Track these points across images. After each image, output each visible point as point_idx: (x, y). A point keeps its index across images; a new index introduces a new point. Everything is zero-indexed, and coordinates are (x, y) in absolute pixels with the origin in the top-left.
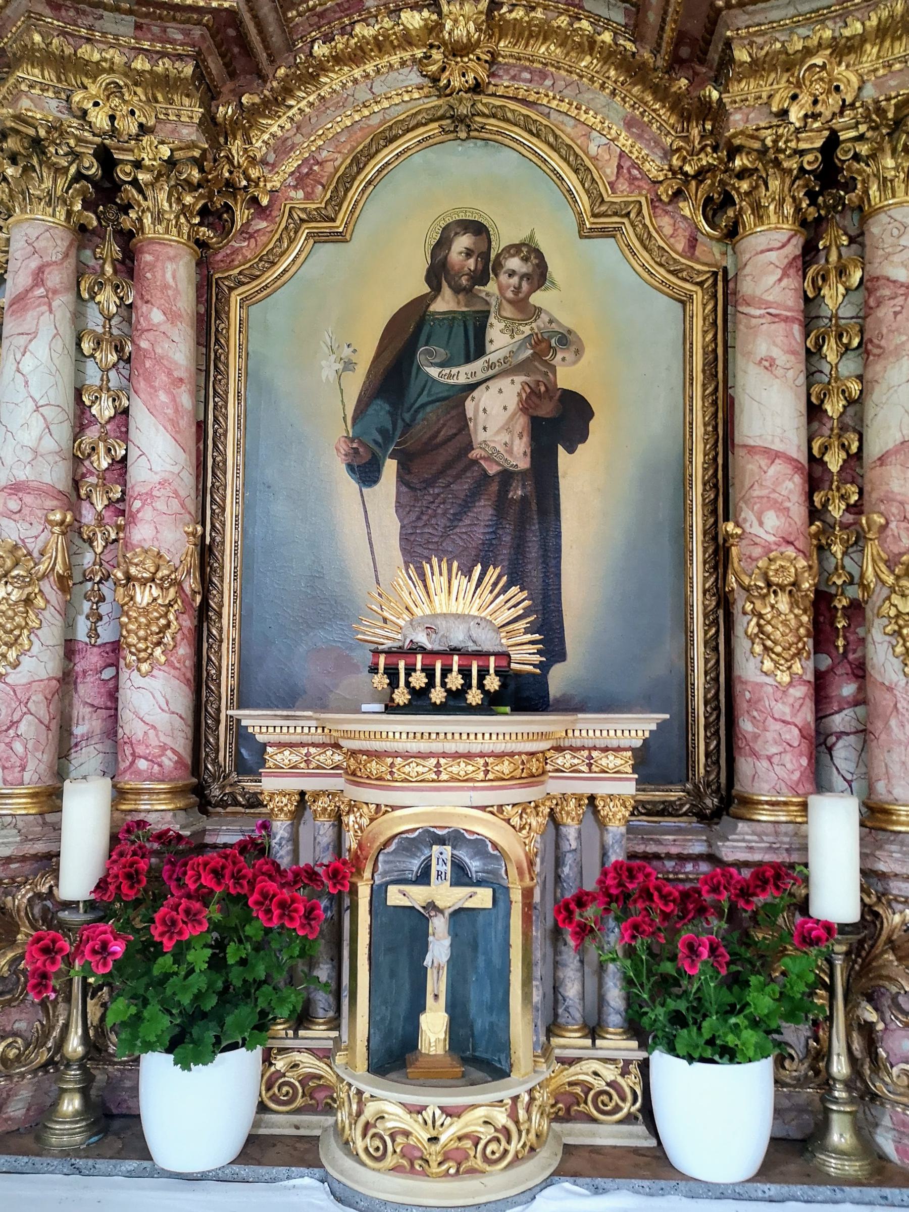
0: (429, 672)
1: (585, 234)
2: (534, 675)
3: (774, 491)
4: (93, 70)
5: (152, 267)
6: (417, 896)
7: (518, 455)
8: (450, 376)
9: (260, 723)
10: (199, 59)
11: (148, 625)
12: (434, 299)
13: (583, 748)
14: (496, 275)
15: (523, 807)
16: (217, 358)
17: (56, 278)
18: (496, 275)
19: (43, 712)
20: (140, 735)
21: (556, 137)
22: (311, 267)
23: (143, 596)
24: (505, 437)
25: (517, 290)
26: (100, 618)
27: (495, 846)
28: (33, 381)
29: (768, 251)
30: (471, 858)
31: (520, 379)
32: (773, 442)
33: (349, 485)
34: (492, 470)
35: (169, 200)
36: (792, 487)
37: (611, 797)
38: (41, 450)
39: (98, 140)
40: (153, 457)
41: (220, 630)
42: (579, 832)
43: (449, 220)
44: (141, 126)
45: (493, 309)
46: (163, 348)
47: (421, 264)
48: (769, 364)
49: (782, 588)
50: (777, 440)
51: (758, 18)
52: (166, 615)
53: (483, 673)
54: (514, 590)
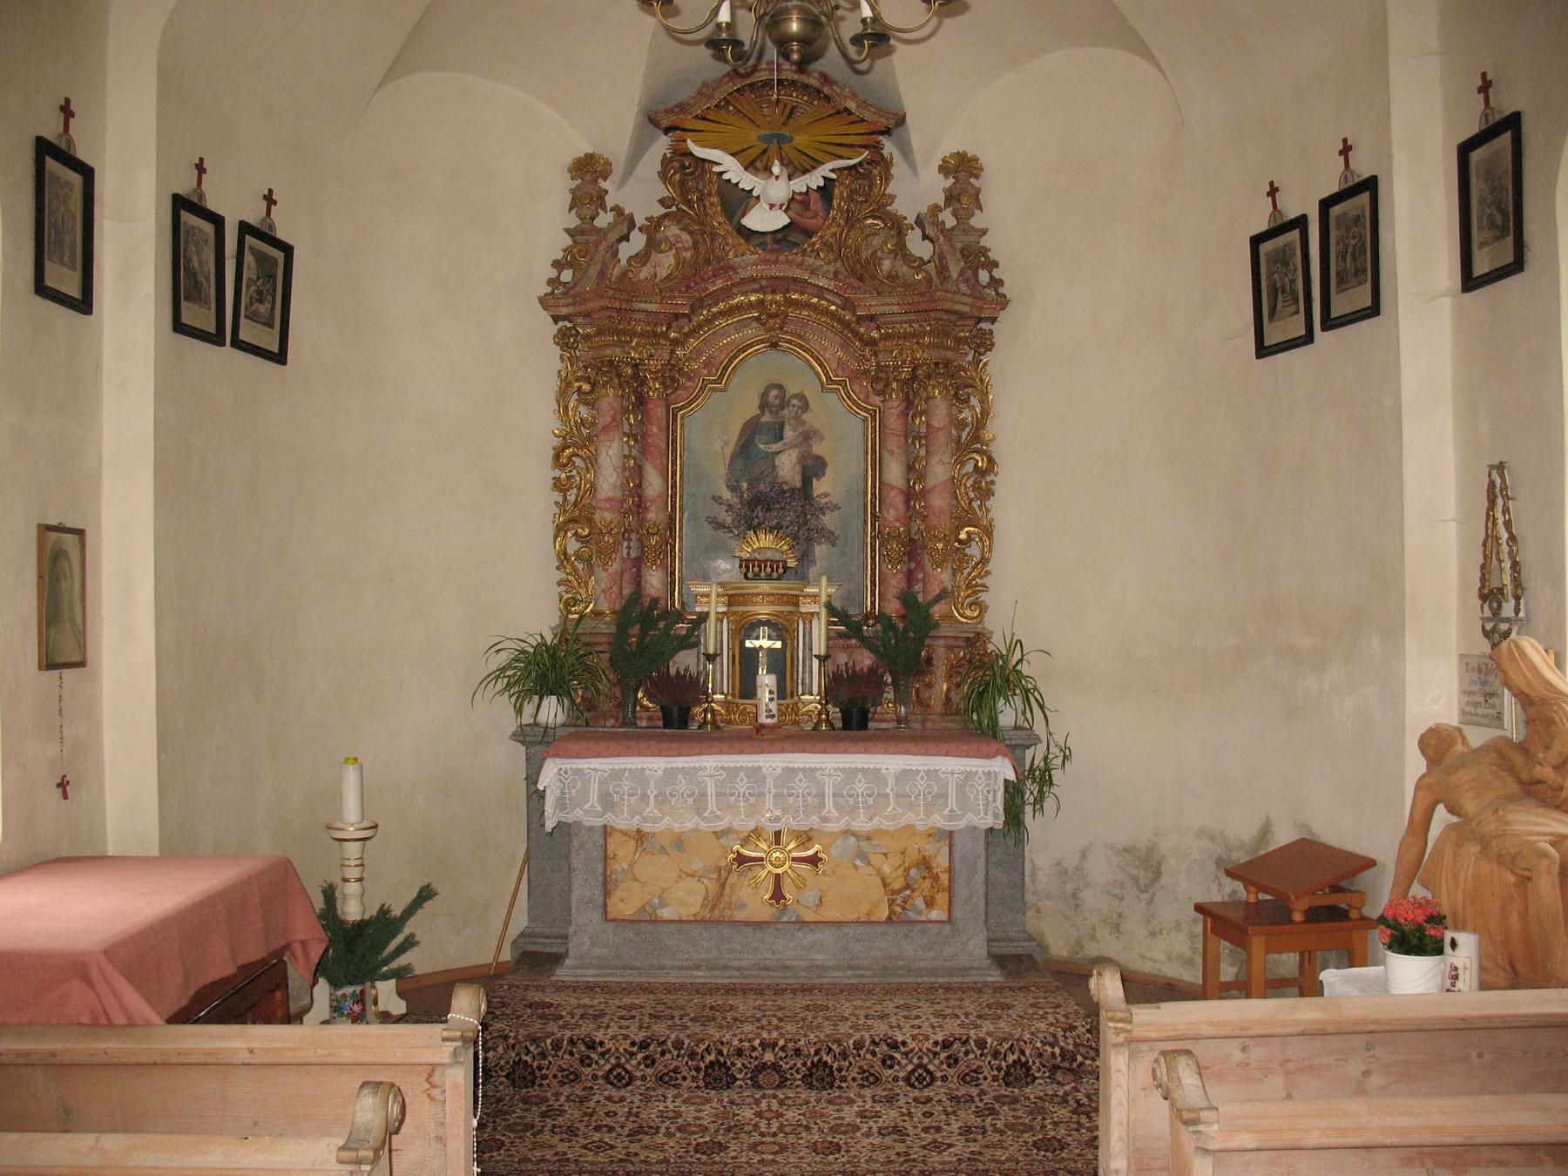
6: (757, 643)
47: (756, 401)
48: (891, 453)
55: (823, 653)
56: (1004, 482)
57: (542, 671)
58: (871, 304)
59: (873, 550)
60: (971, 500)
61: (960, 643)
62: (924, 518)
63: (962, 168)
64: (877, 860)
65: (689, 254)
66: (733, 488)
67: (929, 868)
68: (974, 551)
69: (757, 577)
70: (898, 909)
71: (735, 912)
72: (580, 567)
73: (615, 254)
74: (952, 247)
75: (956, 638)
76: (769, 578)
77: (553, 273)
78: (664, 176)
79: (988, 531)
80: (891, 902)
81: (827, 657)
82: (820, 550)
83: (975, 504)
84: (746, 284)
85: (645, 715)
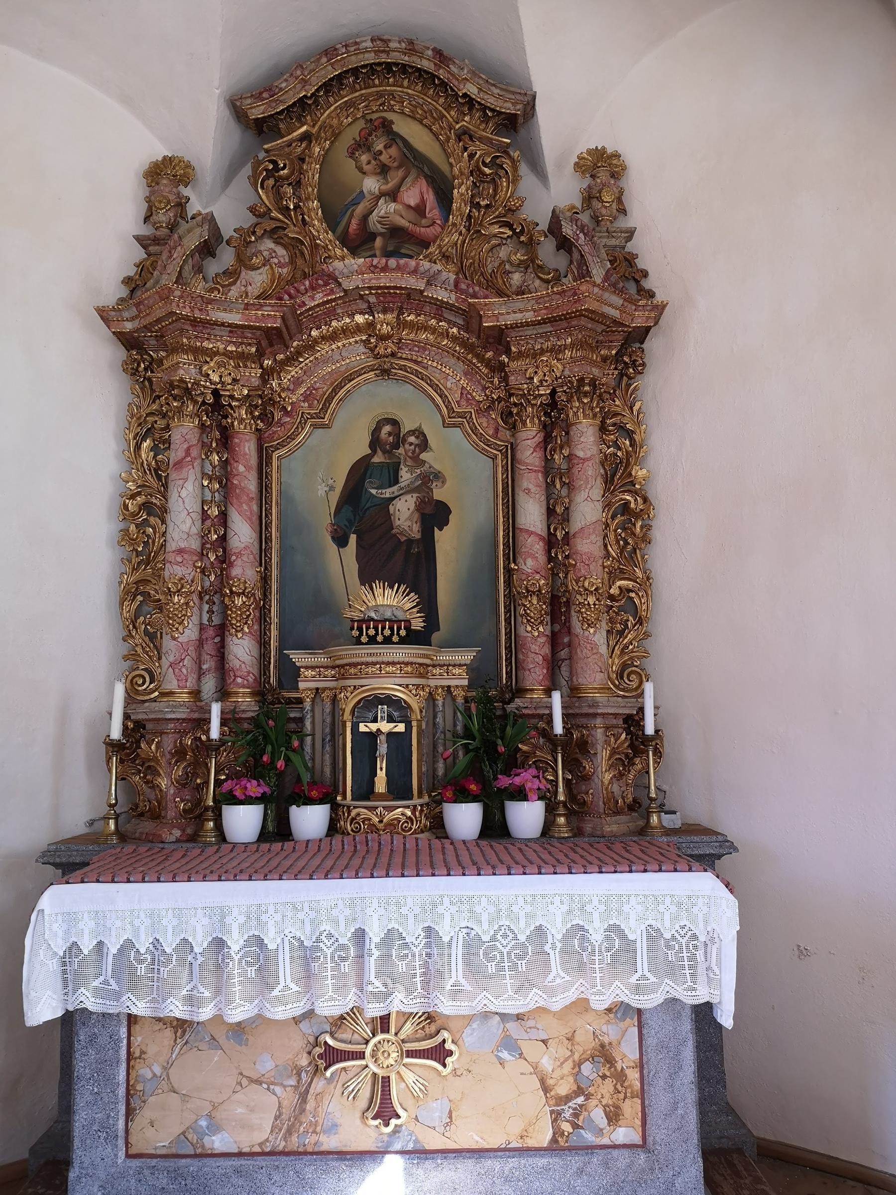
0: (376, 629)
1: (445, 425)
2: (419, 631)
4: (213, 354)
5: (239, 446)
6: (374, 727)
8: (382, 494)
9: (298, 657)
10: (259, 344)
11: (241, 615)
13: (444, 665)
15: (417, 686)
17: (194, 452)
19: (194, 655)
20: (238, 667)
21: (431, 380)
22: (311, 439)
23: (239, 601)
24: (409, 523)
25: (414, 452)
26: (213, 613)
27: (405, 702)
28: (187, 501)
29: (530, 436)
31: (415, 495)
33: (332, 547)
34: (403, 539)
35: (246, 414)
37: (457, 686)
38: (191, 533)
39: (213, 386)
41: (270, 618)
42: (444, 703)
43: (380, 418)
44: (233, 379)
47: (366, 439)
48: (528, 491)
49: (534, 593)
51: (520, 334)
52: (248, 610)
53: (399, 629)
54: (412, 594)
64: (532, 1050)
65: (285, 270)
67: (610, 1061)
70: (567, 1127)
71: (323, 1138)
74: (594, 245)
80: (556, 1116)
84: (353, 299)
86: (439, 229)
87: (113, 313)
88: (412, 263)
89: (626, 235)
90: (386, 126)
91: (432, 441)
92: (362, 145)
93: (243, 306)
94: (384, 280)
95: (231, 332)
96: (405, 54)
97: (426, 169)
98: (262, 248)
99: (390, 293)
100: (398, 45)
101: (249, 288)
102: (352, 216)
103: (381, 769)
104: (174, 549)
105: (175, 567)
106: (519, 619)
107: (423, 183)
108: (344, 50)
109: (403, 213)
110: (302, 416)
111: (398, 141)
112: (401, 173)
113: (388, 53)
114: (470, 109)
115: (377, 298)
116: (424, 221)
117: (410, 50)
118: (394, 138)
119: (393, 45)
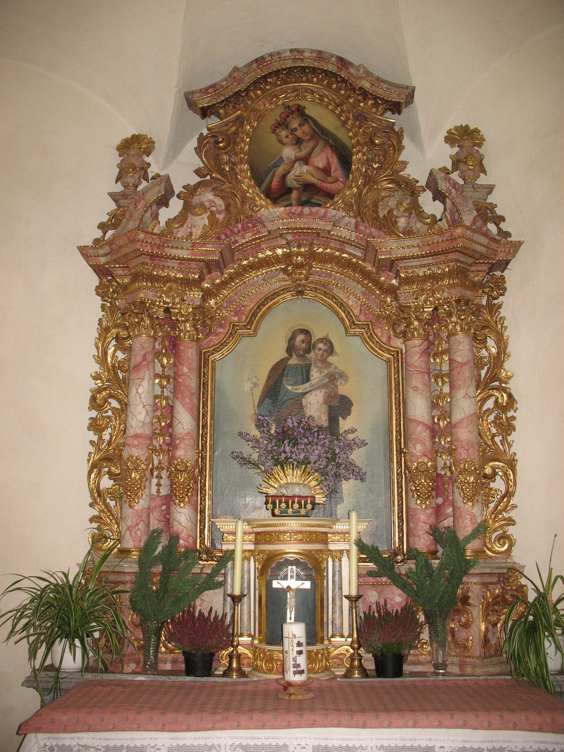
3: (419, 436)
7: (323, 421)
12: (289, 360)
14: (314, 350)
16: (204, 383)
18: (314, 350)
25: (322, 356)
28: (143, 396)
30: (297, 620)
31: (323, 391)
32: (418, 418)
35: (190, 327)
36: (425, 435)
40: (184, 424)
45: (312, 363)
46: (188, 382)
47: (283, 345)
48: (416, 389)
50: (420, 417)
55: (354, 593)
56: (522, 417)
57: (59, 611)
58: (390, 247)
59: (400, 487)
60: (494, 436)
61: (495, 579)
62: (451, 452)
63: (465, 139)
66: (260, 424)
68: (499, 485)
69: (284, 514)
72: (112, 503)
73: (156, 217)
75: (490, 574)
76: (296, 515)
77: (99, 234)
78: (198, 150)
79: (512, 464)
81: (358, 597)
82: (348, 487)
83: (498, 439)
84: (274, 236)
85: (169, 657)
86: (341, 185)
87: (91, 251)
88: (322, 211)
89: (488, 190)
90: (300, 111)
91: (337, 348)
92: (283, 124)
93: (191, 245)
94: (300, 223)
95: (180, 264)
96: (315, 60)
97: (331, 141)
98: (204, 200)
99: (304, 233)
100: (310, 55)
101: (194, 229)
102: (273, 176)
103: (290, 618)
104: (132, 434)
105: (133, 449)
106: (411, 494)
107: (329, 152)
108: (270, 59)
109: (314, 174)
110: (233, 328)
111: (310, 121)
112: (311, 144)
113: (302, 60)
114: (364, 99)
115: (294, 236)
116: (329, 179)
117: (319, 58)
118: (305, 118)
119: (306, 54)
